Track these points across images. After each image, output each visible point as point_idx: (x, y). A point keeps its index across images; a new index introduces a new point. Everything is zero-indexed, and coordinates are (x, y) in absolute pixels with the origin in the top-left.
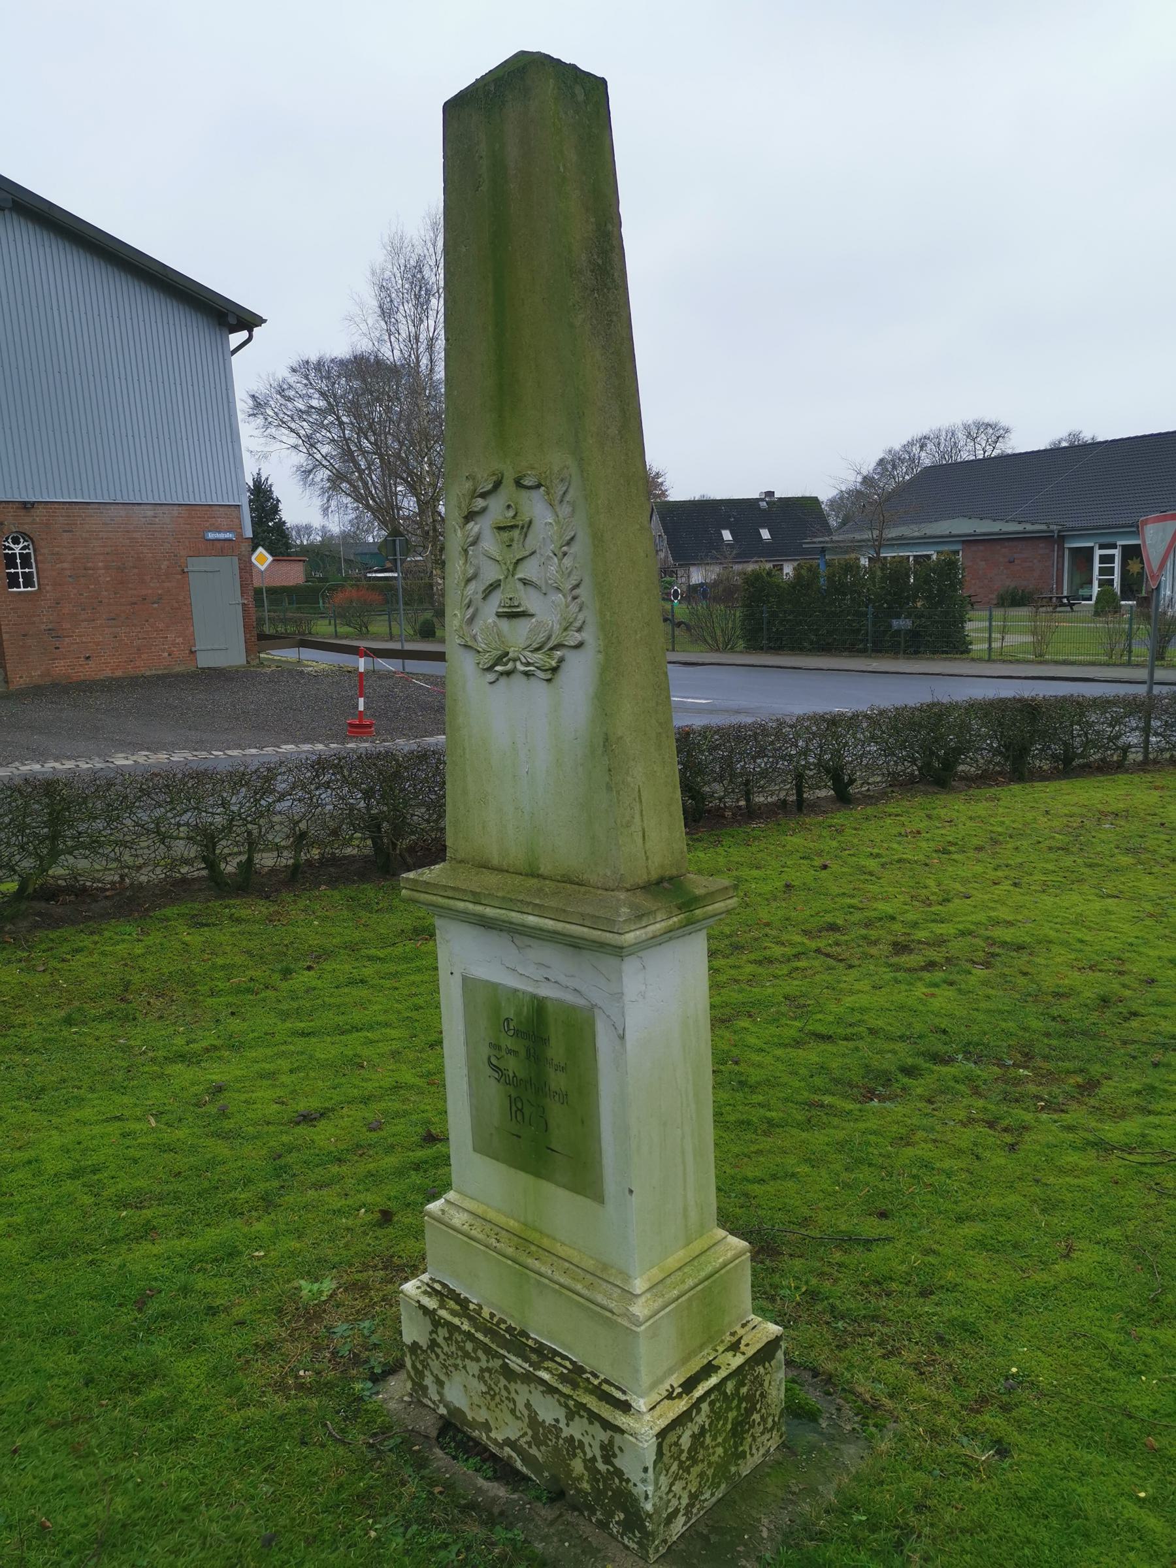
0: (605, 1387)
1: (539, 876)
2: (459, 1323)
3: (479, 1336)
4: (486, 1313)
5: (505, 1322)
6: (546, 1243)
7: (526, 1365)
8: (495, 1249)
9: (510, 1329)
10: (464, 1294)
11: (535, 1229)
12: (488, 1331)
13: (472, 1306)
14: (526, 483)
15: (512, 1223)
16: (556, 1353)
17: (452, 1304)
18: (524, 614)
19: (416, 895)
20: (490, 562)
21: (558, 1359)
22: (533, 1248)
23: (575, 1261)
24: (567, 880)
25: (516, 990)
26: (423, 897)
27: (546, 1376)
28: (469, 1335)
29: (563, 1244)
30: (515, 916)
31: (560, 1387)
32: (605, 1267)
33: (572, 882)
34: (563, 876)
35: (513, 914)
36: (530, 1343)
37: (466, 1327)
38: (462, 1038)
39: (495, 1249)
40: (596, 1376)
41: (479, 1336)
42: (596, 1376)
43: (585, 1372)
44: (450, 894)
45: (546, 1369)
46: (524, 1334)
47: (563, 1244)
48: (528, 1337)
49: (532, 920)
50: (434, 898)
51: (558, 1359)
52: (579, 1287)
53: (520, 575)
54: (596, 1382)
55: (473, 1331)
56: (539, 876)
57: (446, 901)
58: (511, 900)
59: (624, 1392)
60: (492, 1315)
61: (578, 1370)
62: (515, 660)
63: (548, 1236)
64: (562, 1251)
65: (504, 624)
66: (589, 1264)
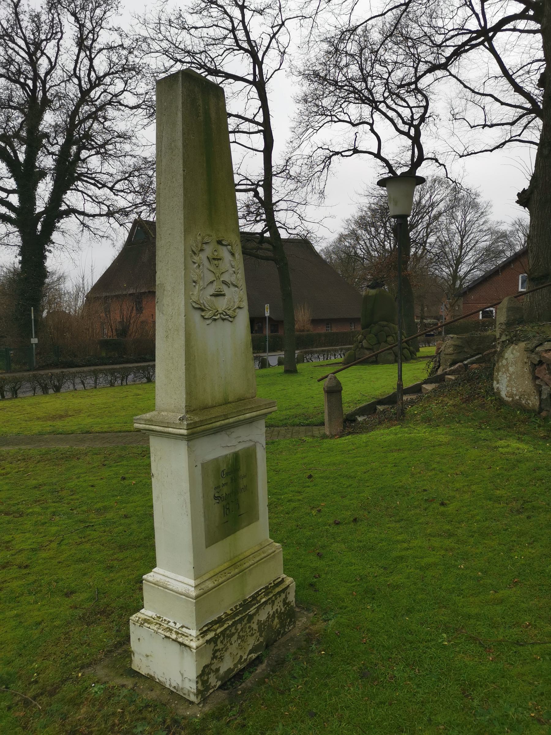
0: (276, 582)
1: (230, 403)
2: (228, 625)
3: (237, 618)
4: (229, 612)
5: (237, 606)
6: (241, 557)
7: (254, 607)
8: (233, 576)
9: (241, 605)
10: (215, 618)
11: (234, 558)
12: (236, 615)
13: (223, 617)
14: (223, 243)
15: (225, 565)
16: (257, 592)
17: (215, 627)
18: (224, 295)
19: (195, 430)
20: (209, 272)
21: (260, 593)
22: (239, 564)
23: (253, 551)
24: (240, 400)
25: (226, 455)
26: (199, 429)
27: (263, 600)
28: (234, 624)
29: (245, 552)
30: (242, 417)
31: (269, 597)
32: (261, 544)
33: (241, 400)
34: (238, 399)
35: (241, 417)
36: (249, 600)
37: (230, 623)
38: (201, 495)
39: (233, 576)
40: (271, 584)
41: (237, 618)
42: (271, 584)
43: (268, 586)
44: (214, 420)
45: (261, 599)
46: (245, 601)
47: (245, 552)
48: (247, 600)
49: (248, 415)
50: (205, 427)
51: (260, 593)
52: (263, 555)
53: (222, 279)
54: (273, 584)
55: (234, 620)
56: (230, 403)
57: (211, 425)
58: (240, 411)
59: (280, 578)
60: (231, 610)
61: (266, 588)
62: (220, 314)
63: (239, 555)
64: (247, 554)
65: (213, 298)
66: (257, 548)
